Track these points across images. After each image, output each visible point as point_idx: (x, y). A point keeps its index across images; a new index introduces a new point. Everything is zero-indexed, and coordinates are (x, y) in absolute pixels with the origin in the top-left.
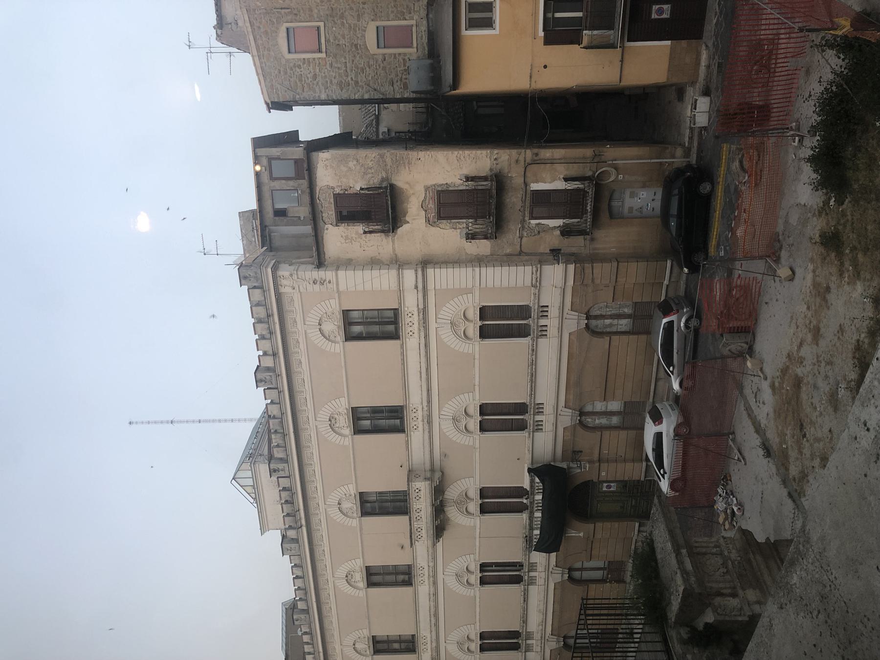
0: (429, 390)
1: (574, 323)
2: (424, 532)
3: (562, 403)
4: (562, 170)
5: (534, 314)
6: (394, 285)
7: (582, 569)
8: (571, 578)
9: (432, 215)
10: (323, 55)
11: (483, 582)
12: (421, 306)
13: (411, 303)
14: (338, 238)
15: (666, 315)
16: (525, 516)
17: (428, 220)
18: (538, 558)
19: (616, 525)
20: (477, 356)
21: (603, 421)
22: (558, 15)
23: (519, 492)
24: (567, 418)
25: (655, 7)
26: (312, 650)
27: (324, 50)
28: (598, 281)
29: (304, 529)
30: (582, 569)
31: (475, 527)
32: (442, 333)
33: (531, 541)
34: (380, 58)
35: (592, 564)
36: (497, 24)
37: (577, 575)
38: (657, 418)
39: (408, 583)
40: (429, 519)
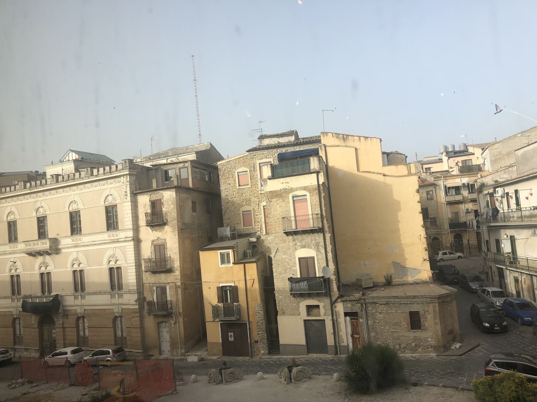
0: (88, 245)
1: (116, 310)
2: (29, 247)
3: (86, 308)
4: (174, 300)
5: (119, 292)
6: (126, 227)
7: (20, 324)
8: (116, 317)
9: (155, 243)
10: (238, 188)
11: (111, 269)
12: (120, 240)
13: (121, 235)
14: (144, 200)
15: (113, 351)
16: (40, 294)
17: (153, 241)
18: (20, 304)
19: (38, 338)
20: (102, 267)
21: (81, 328)
22: (228, 291)
23: (50, 291)
24: (79, 310)
25: (232, 334)
26: (17, 189)
27: (240, 187)
28: (133, 319)
29: (29, 191)
30: (20, 324)
31: (34, 271)
32: (109, 250)
33: (26, 298)
34: (238, 213)
35: (22, 329)
36: (223, 266)
37: (17, 322)
38: (73, 352)
39: (10, 241)
40: (34, 249)
